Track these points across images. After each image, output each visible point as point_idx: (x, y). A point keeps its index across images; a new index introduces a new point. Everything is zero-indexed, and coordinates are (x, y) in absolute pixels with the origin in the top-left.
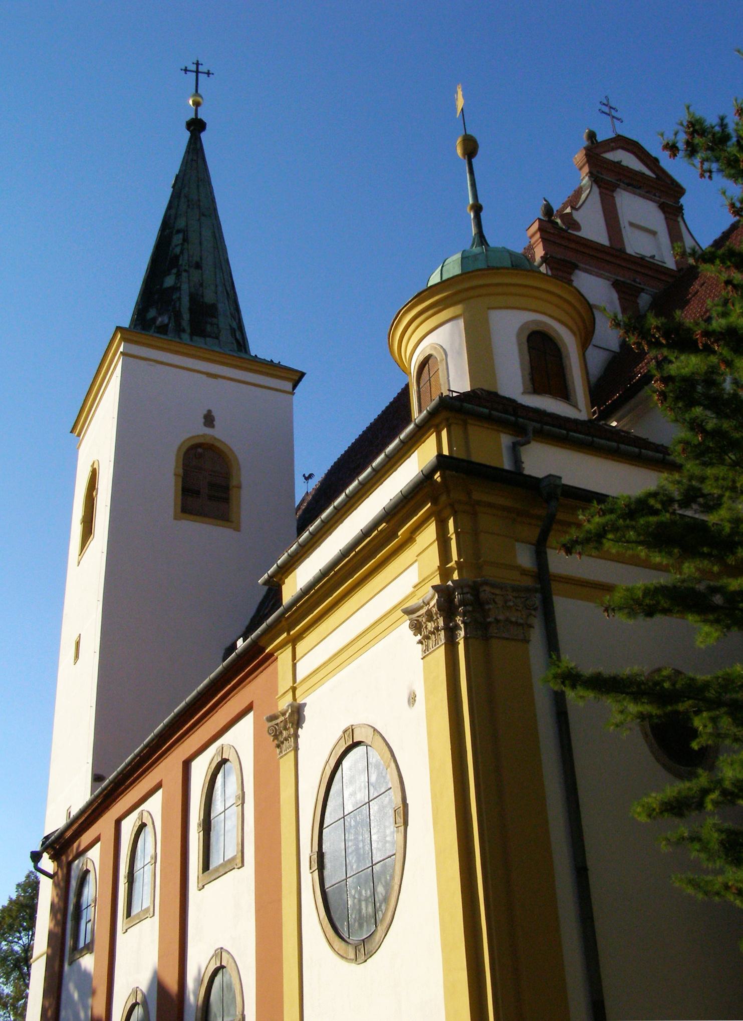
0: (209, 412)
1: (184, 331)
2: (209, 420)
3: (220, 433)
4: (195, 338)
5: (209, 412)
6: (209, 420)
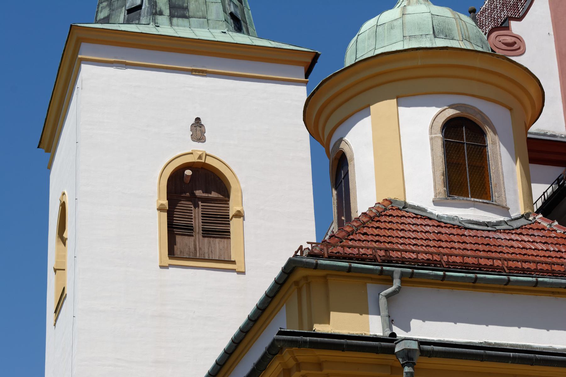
0: (198, 119)
1: (161, 13)
2: (198, 129)
3: (218, 150)
4: (175, 20)
5: (198, 119)
6: (198, 129)
